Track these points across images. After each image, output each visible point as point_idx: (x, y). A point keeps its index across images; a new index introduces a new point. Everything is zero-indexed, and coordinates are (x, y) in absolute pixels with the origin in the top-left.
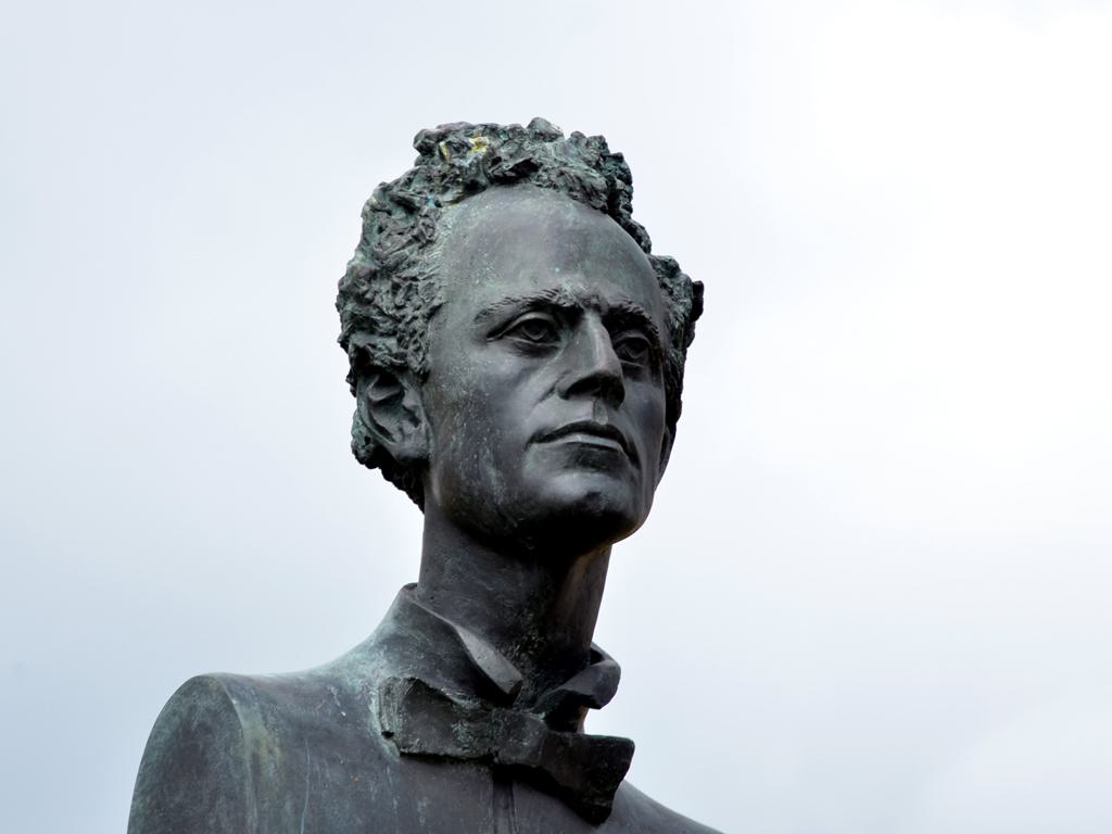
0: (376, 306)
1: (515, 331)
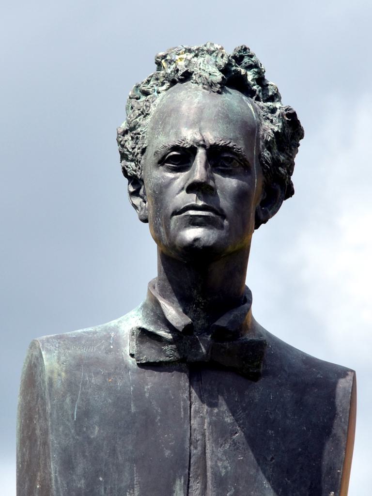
1: (168, 161)
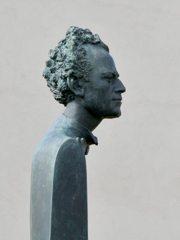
0: (79, 66)
